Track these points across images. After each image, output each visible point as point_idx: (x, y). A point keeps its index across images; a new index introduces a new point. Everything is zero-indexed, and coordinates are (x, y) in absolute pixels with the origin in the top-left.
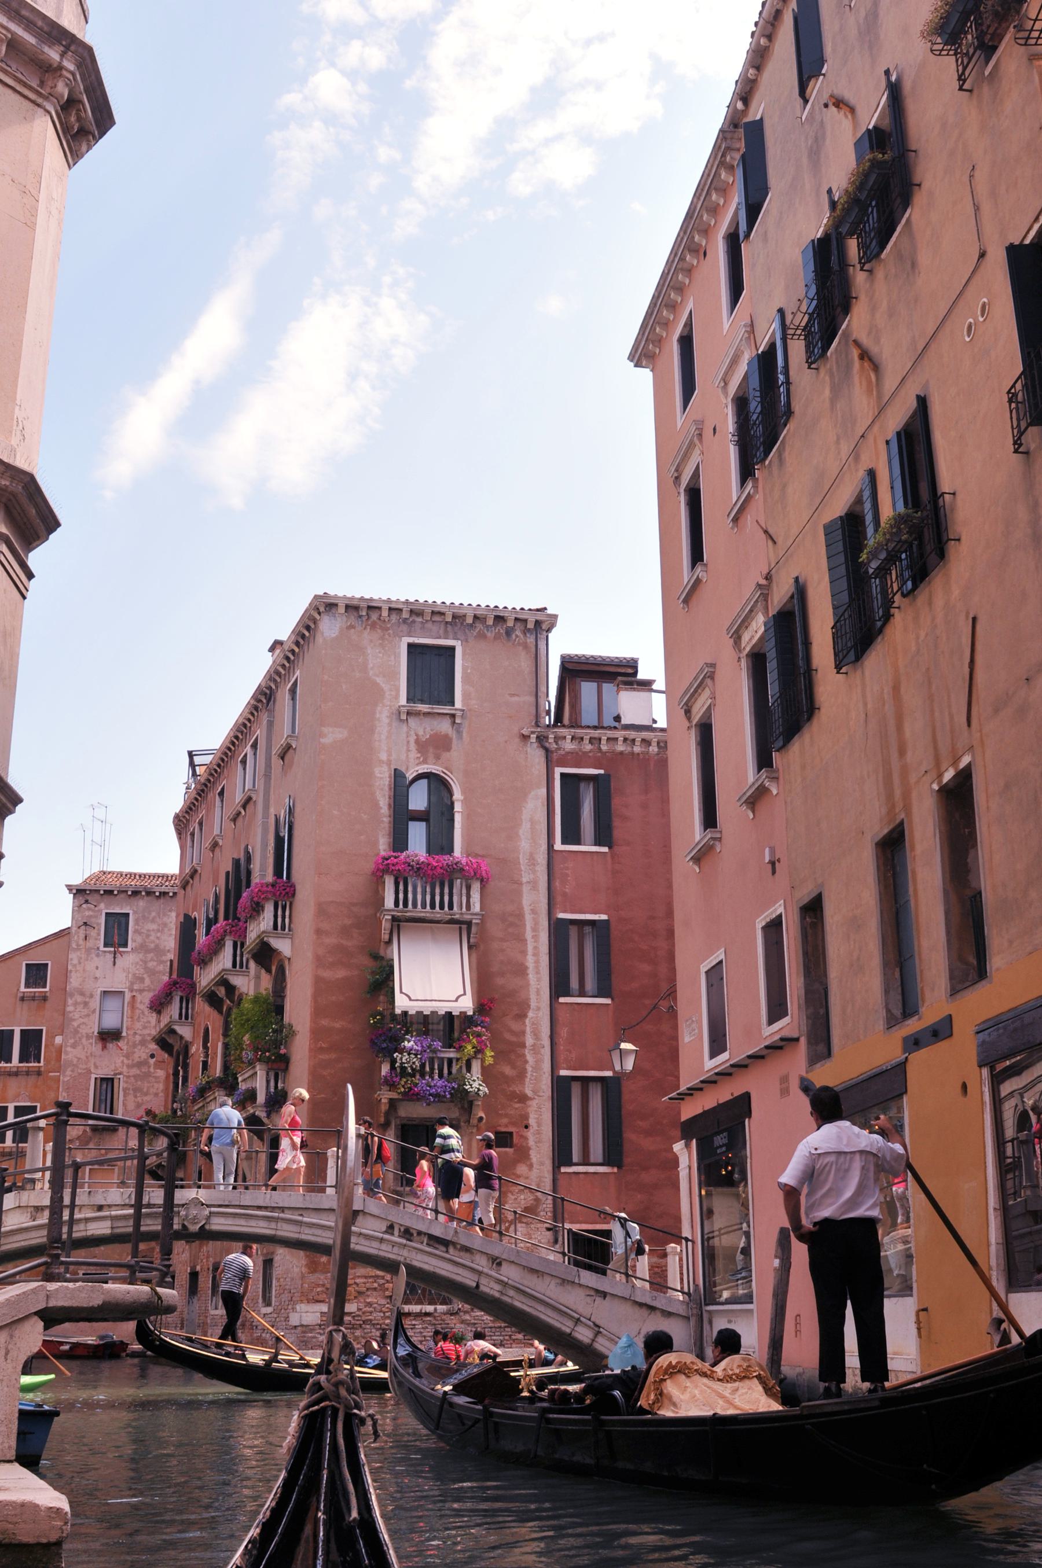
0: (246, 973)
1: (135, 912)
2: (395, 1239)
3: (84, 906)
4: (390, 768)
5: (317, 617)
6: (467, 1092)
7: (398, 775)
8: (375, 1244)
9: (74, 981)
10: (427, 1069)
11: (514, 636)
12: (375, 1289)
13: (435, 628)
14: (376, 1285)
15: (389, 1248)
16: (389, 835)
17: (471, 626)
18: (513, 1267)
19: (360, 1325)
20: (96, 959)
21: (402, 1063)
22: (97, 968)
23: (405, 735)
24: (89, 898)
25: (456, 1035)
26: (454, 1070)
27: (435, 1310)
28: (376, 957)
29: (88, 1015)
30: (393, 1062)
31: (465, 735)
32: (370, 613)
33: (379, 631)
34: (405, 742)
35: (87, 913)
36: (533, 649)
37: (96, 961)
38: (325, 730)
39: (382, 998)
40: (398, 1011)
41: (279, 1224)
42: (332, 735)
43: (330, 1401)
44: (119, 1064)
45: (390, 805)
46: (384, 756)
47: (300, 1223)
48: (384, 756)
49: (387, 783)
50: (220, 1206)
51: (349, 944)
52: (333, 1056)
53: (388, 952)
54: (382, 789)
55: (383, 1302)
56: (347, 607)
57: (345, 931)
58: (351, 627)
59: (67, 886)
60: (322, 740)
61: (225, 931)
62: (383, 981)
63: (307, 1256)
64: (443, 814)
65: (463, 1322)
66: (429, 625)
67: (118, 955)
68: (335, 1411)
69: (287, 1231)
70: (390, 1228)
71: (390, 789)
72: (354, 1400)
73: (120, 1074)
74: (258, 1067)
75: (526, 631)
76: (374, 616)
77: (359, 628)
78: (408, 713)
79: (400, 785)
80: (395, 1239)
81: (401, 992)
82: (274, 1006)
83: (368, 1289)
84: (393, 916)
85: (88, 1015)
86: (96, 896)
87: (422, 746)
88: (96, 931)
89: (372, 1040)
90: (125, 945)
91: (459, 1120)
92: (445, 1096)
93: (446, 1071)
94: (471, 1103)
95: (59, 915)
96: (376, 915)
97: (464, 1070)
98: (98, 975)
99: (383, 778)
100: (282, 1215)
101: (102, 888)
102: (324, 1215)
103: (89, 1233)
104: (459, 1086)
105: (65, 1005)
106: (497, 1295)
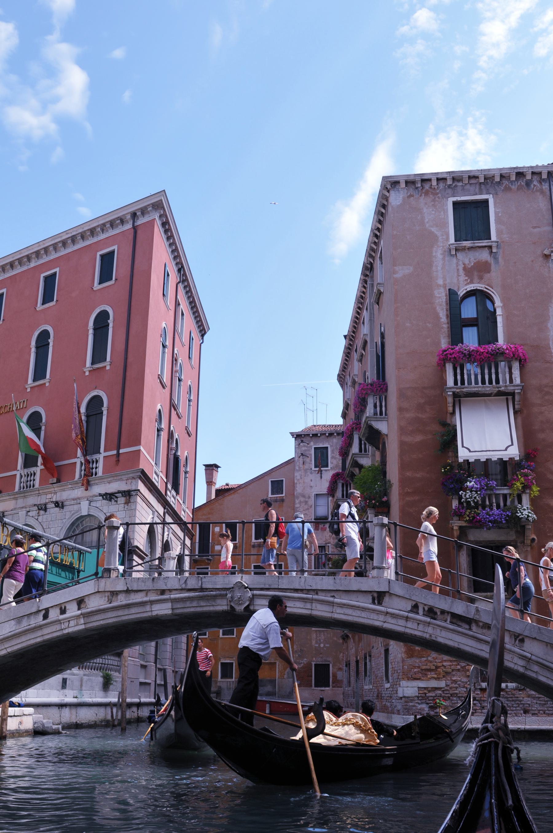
0: (367, 456)
1: (331, 446)
2: (420, 617)
3: (301, 444)
4: (445, 289)
5: (387, 194)
6: (520, 519)
7: (452, 293)
8: (402, 622)
9: (299, 489)
10: (487, 503)
11: (532, 186)
12: (459, 670)
13: (472, 188)
14: (459, 667)
15: (415, 626)
16: (448, 336)
17: (499, 183)
18: (536, 643)
19: (449, 697)
20: (310, 475)
21: (467, 499)
22: (311, 480)
23: (455, 265)
24: (304, 440)
25: (509, 478)
26: (508, 503)
27: (507, 686)
28: (444, 424)
29: (308, 509)
30: (460, 498)
31: (500, 260)
32: (424, 184)
33: (431, 196)
34: (456, 271)
35: (303, 449)
36: (548, 193)
37: (311, 477)
38: (397, 268)
39: (450, 454)
40: (461, 460)
41: (314, 605)
42: (402, 271)
43: (494, 738)
44: (328, 537)
45: (447, 315)
46: (440, 282)
47: (332, 604)
48: (440, 282)
49: (444, 300)
50: (262, 589)
51: (424, 417)
52: (417, 498)
53: (453, 420)
54: (441, 305)
55: (465, 680)
56: (407, 183)
57: (420, 408)
58: (411, 196)
59: (291, 433)
60: (395, 276)
61: (353, 428)
62: (449, 441)
63: (405, 646)
64: (488, 318)
65: (529, 696)
66: (468, 187)
67: (323, 472)
68: (497, 744)
69: (321, 611)
70: (415, 608)
71: (447, 304)
72: (507, 739)
73: (329, 543)
74: (369, 512)
75: (541, 181)
76: (427, 186)
77: (416, 196)
78: (457, 250)
79: (454, 301)
80: (420, 617)
81: (463, 446)
82: (381, 471)
83: (453, 670)
84: (454, 393)
85: (308, 509)
86: (309, 438)
87: (469, 272)
88: (309, 459)
89: (443, 484)
90: (327, 466)
91: (516, 542)
92: (501, 522)
93: (502, 504)
94: (523, 527)
95: (287, 450)
96: (442, 394)
97: (516, 502)
98: (312, 485)
99: (441, 298)
100: (315, 597)
101: (311, 433)
102: (354, 596)
103: (154, 613)
104: (512, 514)
105: (294, 503)
106: (521, 670)
